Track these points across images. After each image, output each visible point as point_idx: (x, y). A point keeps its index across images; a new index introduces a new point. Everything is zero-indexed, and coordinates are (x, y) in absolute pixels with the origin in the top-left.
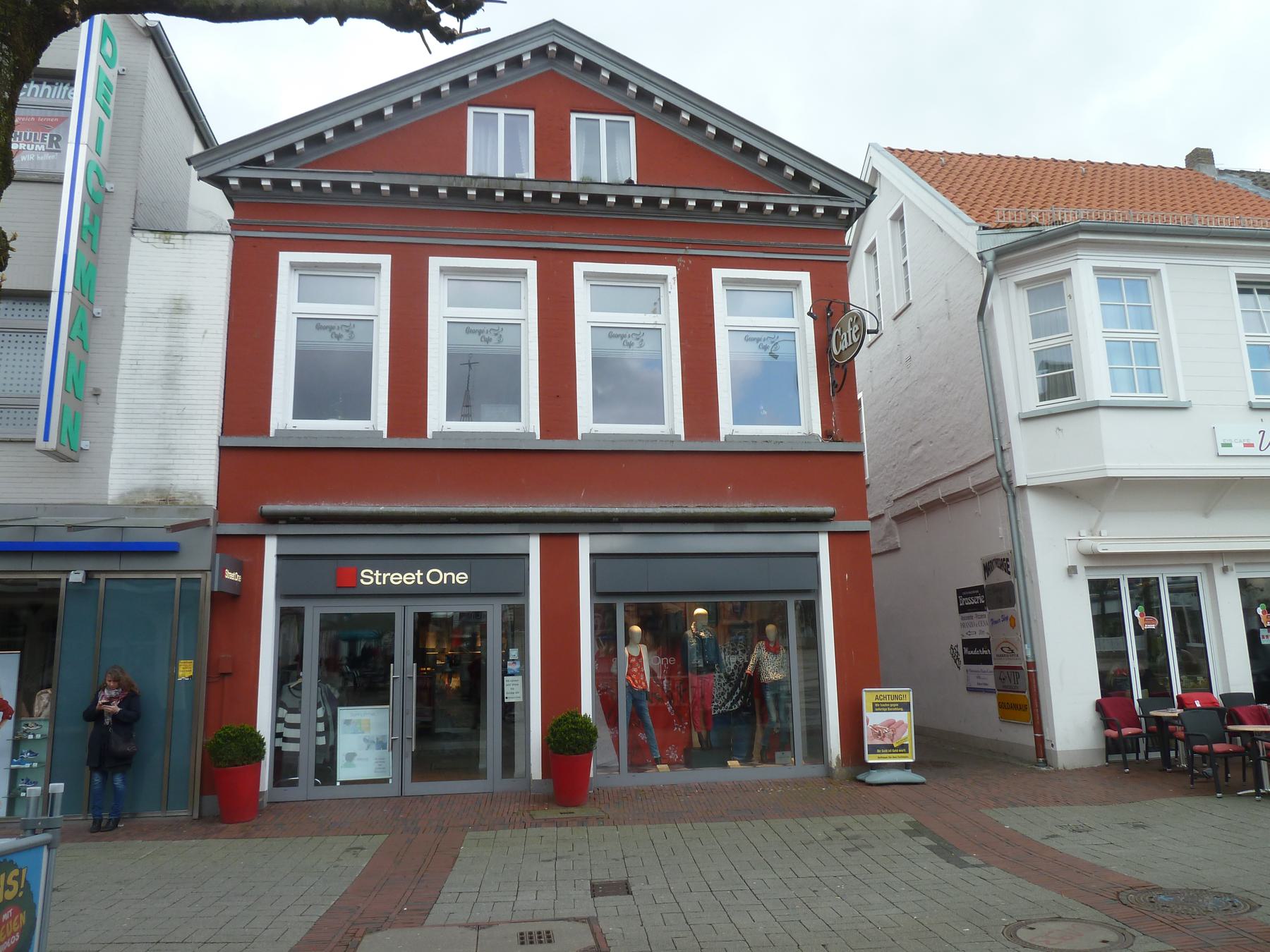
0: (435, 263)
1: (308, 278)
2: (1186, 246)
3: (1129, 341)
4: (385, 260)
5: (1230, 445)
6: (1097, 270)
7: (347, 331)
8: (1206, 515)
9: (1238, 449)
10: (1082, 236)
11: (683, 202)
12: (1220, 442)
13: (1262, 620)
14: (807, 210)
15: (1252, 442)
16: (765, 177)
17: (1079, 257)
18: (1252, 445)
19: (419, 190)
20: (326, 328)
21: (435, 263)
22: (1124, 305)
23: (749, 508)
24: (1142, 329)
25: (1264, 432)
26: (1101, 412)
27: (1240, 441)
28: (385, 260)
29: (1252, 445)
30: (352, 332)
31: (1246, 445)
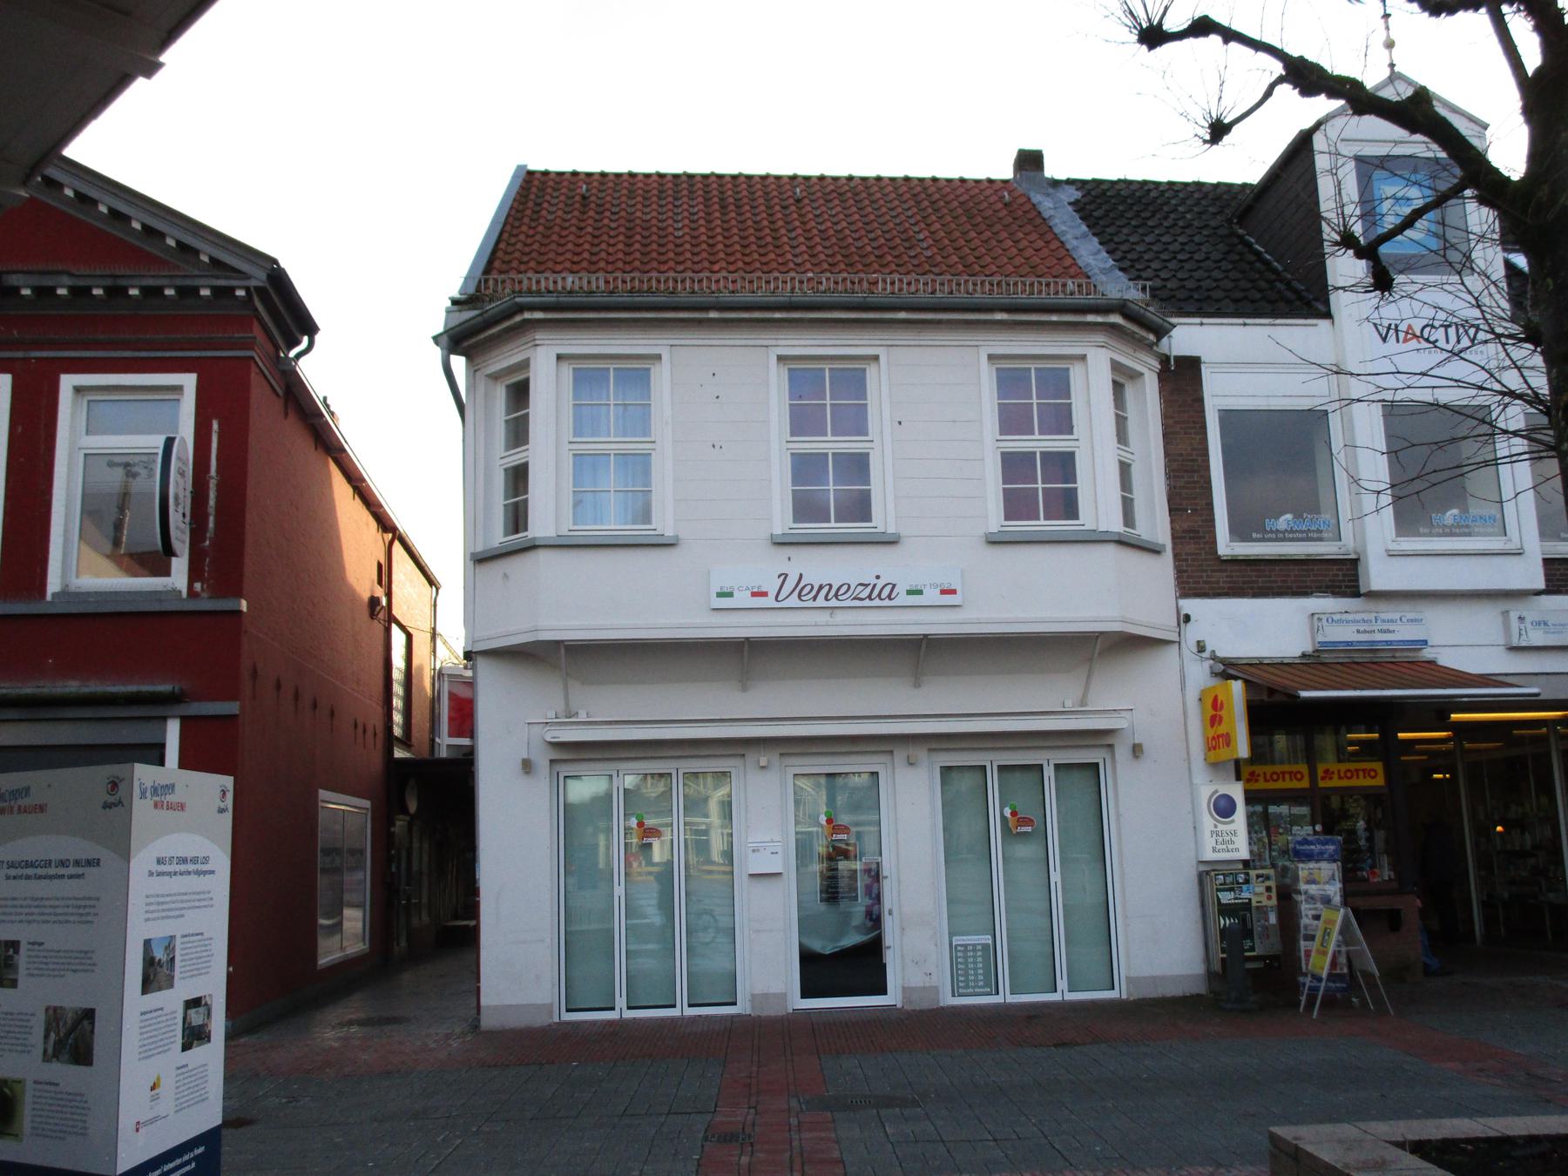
0: (68, 382)
1: (102, 404)
2: (940, 322)
3: (610, 455)
4: (189, 381)
5: (730, 595)
6: (781, 359)
7: (146, 467)
8: (745, 689)
9: (742, 599)
10: (527, 315)
11: (158, 291)
12: (716, 589)
13: (1010, 825)
14: (186, 292)
15: (765, 590)
16: (148, 249)
17: (537, 342)
18: (764, 594)
19: (69, 291)
20: (118, 465)
21: (68, 382)
22: (609, 405)
23: (72, 687)
24: (624, 436)
25: (787, 575)
26: (542, 556)
27: (747, 589)
28: (189, 381)
29: (764, 594)
30: (151, 469)
31: (943, 592)
